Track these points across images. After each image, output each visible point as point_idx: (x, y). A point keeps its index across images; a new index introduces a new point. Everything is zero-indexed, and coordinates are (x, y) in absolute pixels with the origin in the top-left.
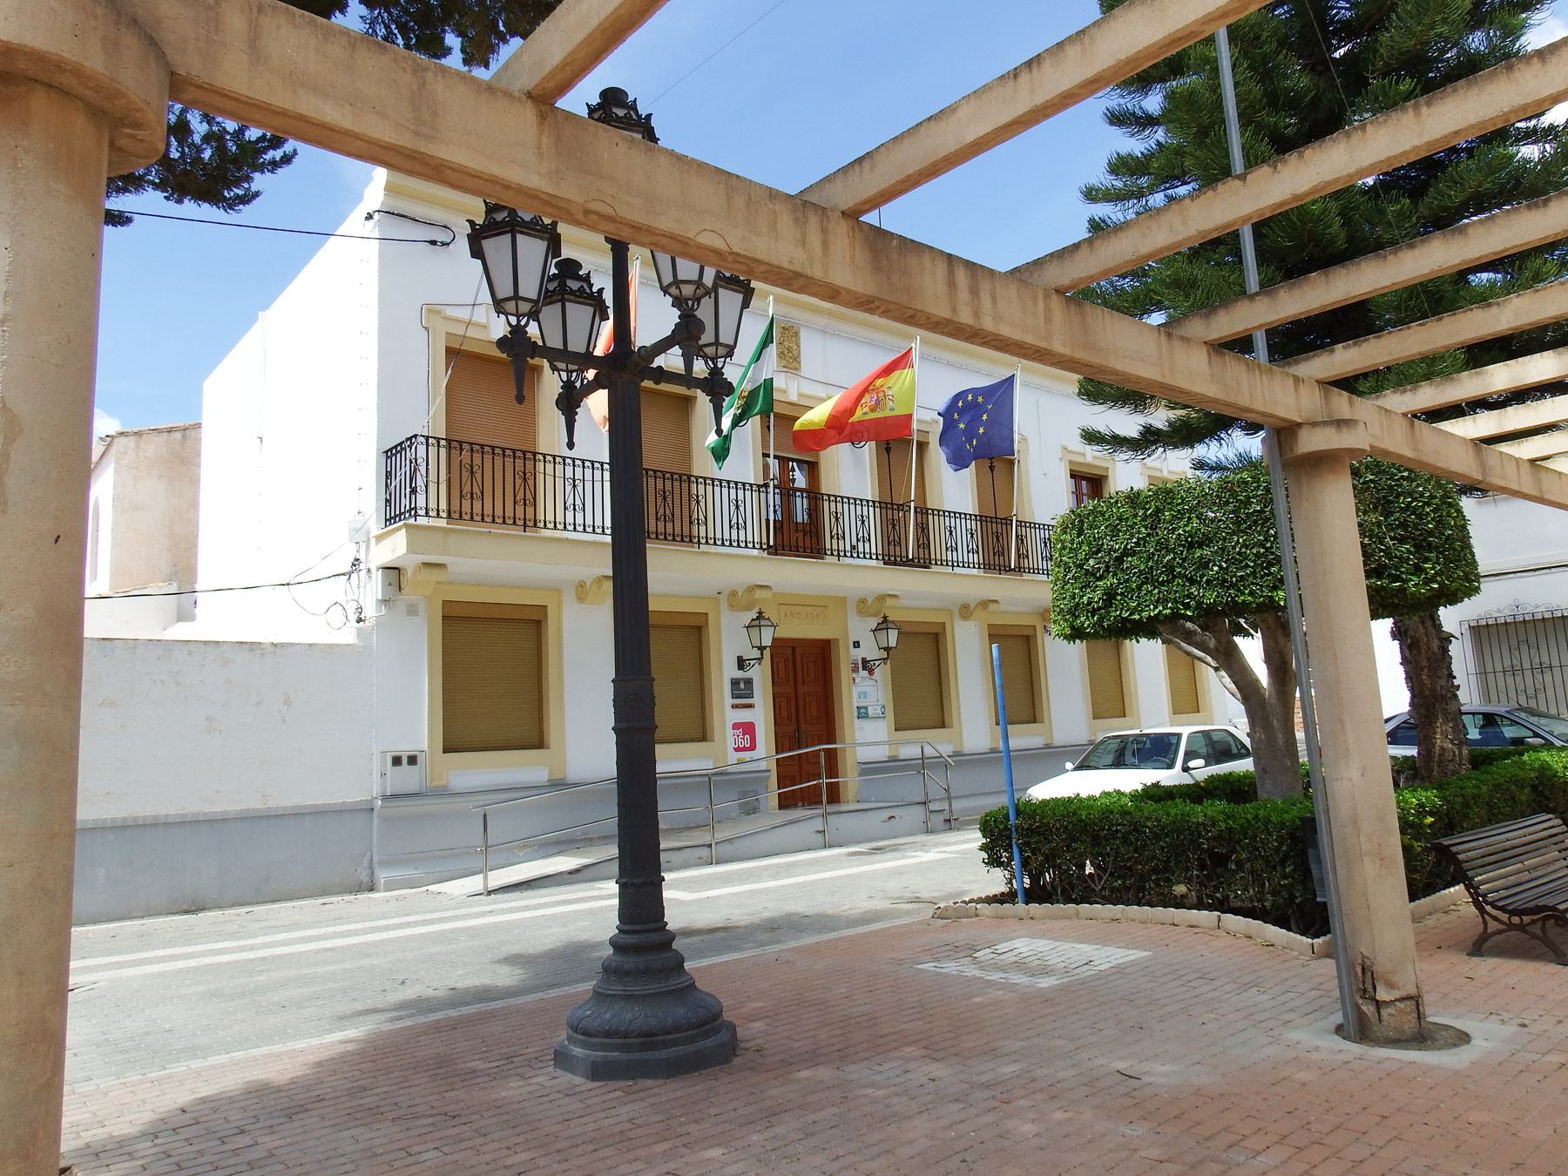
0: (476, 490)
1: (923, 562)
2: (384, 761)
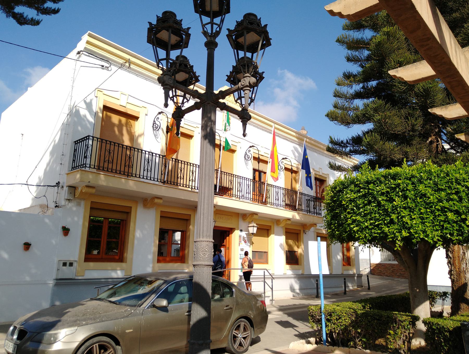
0: (111, 159)
1: (265, 203)
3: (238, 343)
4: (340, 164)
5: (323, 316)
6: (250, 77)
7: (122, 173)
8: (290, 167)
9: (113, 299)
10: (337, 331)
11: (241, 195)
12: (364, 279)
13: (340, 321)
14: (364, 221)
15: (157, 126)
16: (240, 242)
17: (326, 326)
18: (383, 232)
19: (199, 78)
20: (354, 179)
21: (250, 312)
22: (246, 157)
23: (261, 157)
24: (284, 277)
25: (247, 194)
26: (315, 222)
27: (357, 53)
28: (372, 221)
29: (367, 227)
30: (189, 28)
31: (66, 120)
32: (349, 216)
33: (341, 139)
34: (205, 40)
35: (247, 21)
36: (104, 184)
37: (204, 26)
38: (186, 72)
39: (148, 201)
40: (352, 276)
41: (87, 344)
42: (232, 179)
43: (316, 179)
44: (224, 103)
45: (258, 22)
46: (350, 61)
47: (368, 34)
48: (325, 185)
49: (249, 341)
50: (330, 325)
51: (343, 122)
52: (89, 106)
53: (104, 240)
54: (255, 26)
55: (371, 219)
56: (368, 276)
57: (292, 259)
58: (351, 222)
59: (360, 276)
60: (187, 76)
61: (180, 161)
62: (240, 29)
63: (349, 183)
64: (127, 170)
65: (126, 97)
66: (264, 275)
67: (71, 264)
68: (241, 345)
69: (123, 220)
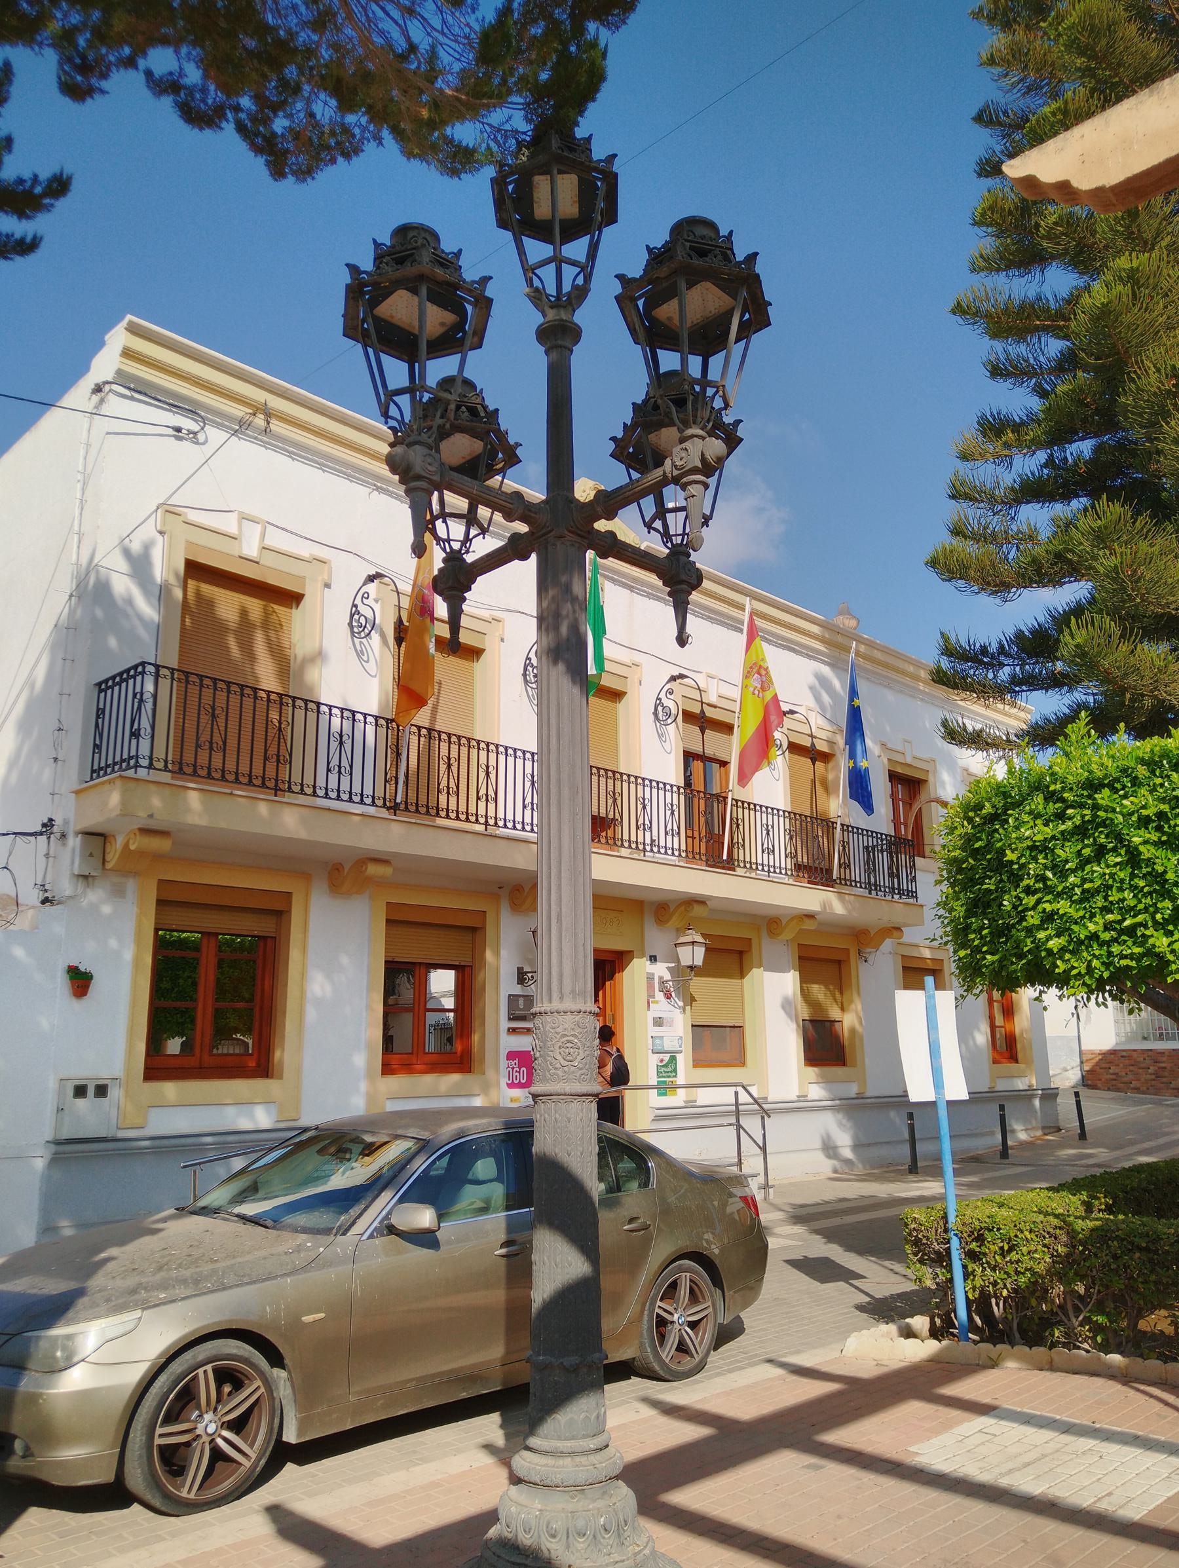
0: (217, 738)
1: (729, 865)
2: (61, 1091)
3: (672, 1341)
4: (978, 726)
5: (955, 1243)
6: (703, 438)
7: (258, 782)
8: (807, 742)
9: (250, 1209)
10: (1005, 1293)
11: (648, 841)
12: (1066, 1105)
13: (1014, 1256)
14: (1083, 917)
15: (363, 620)
16: (651, 995)
17: (966, 1276)
18: (1150, 952)
19: (519, 452)
20: (1043, 775)
21: (708, 1236)
22: (660, 714)
23: (710, 713)
24: (800, 1107)
25: (669, 838)
26: (897, 920)
27: (1022, 349)
28: (1110, 917)
29: (1094, 937)
30: (486, 279)
31: (67, 609)
32: (1030, 901)
33: (982, 640)
34: (537, 319)
35: (688, 244)
36: (202, 821)
37: (529, 271)
38: (474, 434)
39: (345, 873)
40: (1025, 1096)
41: (177, 1367)
42: (618, 789)
43: (894, 777)
44: (612, 534)
45: (725, 248)
46: (1001, 375)
47: (1056, 282)
48: (923, 797)
49: (708, 1333)
50: (979, 1270)
51: (988, 584)
52: (139, 565)
53: (204, 1006)
54: (715, 262)
55: (1106, 910)
56: (1077, 1094)
57: (824, 1046)
58: (1037, 922)
59: (1050, 1095)
60: (478, 446)
61: (444, 736)
62: (664, 271)
63: (1025, 789)
64: (271, 772)
65: (259, 528)
66: (737, 1104)
67: (101, 1091)
68: (682, 1348)
69: (265, 938)
